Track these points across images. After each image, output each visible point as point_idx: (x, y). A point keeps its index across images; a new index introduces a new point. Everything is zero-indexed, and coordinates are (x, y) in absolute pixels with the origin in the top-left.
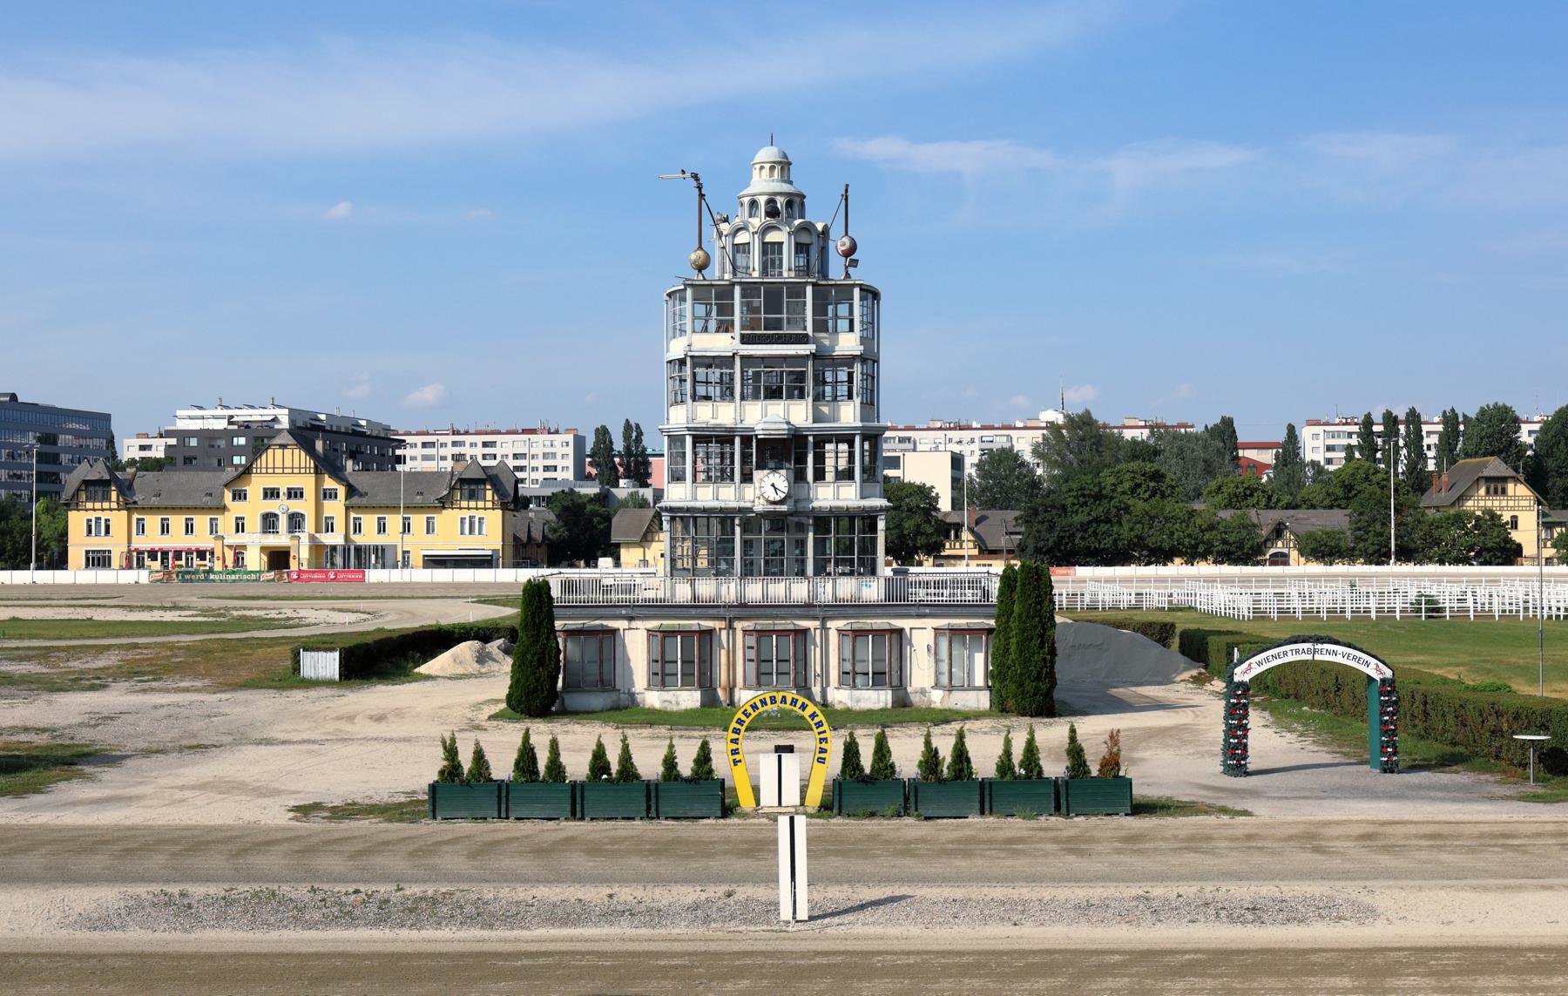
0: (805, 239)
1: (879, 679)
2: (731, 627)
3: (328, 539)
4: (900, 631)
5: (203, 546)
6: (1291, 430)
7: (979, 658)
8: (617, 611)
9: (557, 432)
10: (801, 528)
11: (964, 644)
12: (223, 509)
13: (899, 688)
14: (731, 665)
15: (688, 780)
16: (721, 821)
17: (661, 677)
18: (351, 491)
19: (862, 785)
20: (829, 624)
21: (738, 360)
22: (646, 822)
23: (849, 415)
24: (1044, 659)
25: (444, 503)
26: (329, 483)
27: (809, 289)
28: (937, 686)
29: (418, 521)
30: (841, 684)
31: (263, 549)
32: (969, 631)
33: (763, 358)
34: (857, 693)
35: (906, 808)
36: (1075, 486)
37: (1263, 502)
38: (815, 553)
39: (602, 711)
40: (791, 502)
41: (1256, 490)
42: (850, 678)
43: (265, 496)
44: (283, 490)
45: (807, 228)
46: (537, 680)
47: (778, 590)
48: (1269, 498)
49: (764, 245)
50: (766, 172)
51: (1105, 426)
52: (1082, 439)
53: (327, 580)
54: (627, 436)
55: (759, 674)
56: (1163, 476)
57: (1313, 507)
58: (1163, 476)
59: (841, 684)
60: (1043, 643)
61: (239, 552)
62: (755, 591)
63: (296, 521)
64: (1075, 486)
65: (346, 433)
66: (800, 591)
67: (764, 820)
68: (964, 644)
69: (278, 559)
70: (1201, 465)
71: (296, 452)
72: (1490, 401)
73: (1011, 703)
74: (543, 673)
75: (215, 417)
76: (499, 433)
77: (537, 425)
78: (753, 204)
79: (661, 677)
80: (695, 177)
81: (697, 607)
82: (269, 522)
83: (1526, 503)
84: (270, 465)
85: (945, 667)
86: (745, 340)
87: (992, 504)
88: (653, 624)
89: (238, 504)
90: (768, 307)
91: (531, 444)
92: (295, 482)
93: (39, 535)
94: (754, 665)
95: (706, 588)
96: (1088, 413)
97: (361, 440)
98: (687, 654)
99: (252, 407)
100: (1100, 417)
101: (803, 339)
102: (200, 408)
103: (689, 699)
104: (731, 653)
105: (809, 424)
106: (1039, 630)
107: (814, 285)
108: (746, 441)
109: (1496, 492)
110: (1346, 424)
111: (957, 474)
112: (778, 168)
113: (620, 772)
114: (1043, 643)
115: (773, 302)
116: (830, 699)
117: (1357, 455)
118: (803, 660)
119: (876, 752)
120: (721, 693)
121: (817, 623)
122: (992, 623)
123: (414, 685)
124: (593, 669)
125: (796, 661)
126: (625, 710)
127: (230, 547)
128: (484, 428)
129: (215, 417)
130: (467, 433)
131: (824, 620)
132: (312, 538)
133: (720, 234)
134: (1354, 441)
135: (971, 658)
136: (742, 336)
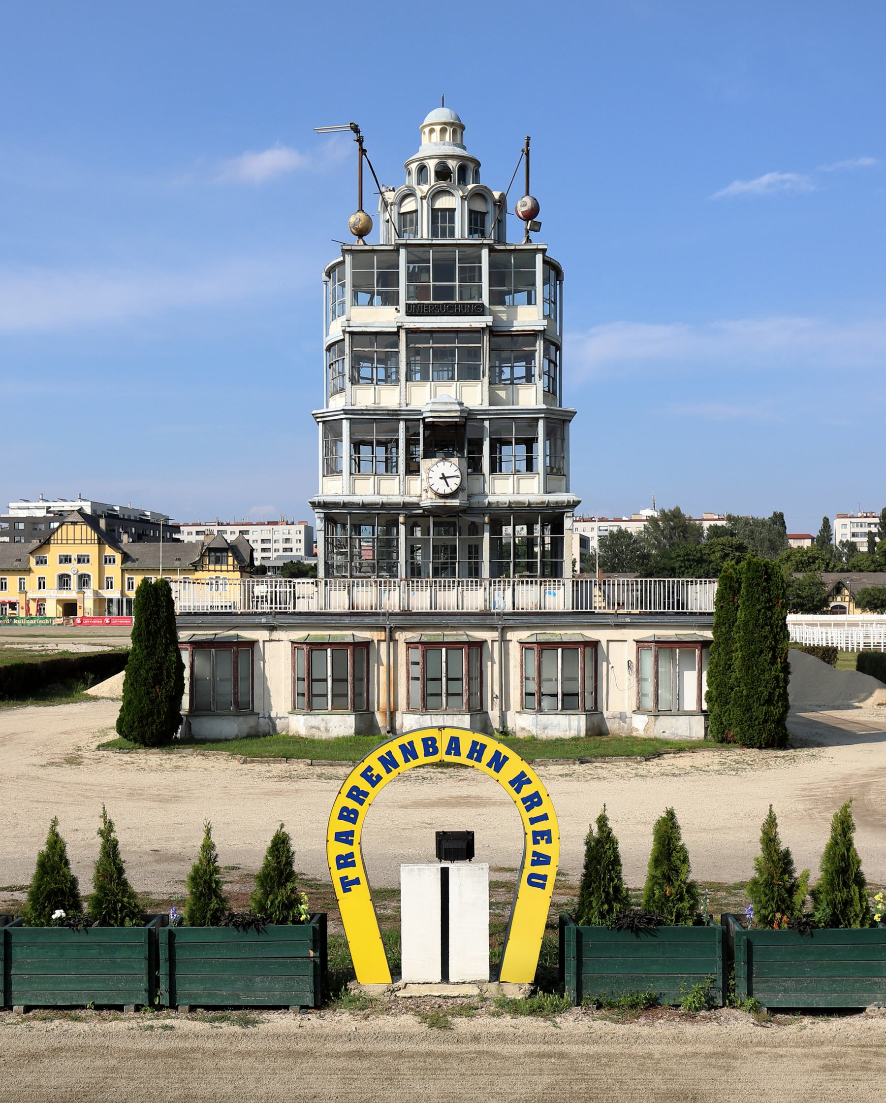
0: (479, 206)
1: (569, 701)
2: (391, 639)
3: (107, 594)
4: (594, 645)
5: (13, 600)
6: (826, 522)
7: (690, 678)
8: (257, 620)
9: (293, 524)
10: (475, 530)
11: (673, 658)
12: (29, 571)
13: (594, 712)
14: (392, 684)
15: (245, 924)
16: (314, 1021)
17: (308, 698)
18: (126, 557)
19: (627, 937)
20: (510, 635)
21: (403, 335)
22: (148, 1019)
23: (530, 397)
24: (777, 678)
25: (196, 566)
26: (109, 551)
27: (485, 253)
28: (639, 710)
30: (524, 707)
31: (59, 601)
32: (680, 643)
33: (431, 332)
34: (543, 719)
35: (727, 989)
36: (682, 553)
37: (823, 567)
38: (492, 556)
39: (236, 738)
40: (463, 496)
41: (817, 558)
42: (534, 700)
43: (61, 562)
44: (74, 557)
45: (481, 194)
46: (152, 701)
47: (449, 599)
48: (828, 565)
49: (434, 212)
50: (436, 136)
51: (690, 519)
52: (673, 528)
53: (104, 624)
55: (425, 696)
56: (746, 548)
57: (861, 571)
58: (746, 548)
59: (525, 707)
60: (774, 657)
61: (41, 604)
62: (420, 600)
63: (84, 580)
64: (682, 553)
65: (135, 521)
66: (474, 599)
67: (408, 1022)
68: (673, 658)
70: (767, 544)
71: (84, 527)
73: (734, 731)
74: (160, 692)
75: (37, 508)
76: (252, 524)
77: (279, 519)
78: (422, 169)
79: (308, 698)
80: (356, 129)
81: (355, 616)
82: (64, 581)
84: (64, 537)
85: (649, 688)
86: (412, 311)
87: (613, 569)
88: (299, 635)
89: (40, 567)
90: (440, 277)
91: (274, 533)
92: (83, 550)
94: (418, 684)
95: (366, 596)
96: (678, 510)
97: (146, 525)
98: (342, 670)
99: (65, 501)
100: (687, 512)
101: (478, 310)
102: (27, 501)
103: (342, 725)
104: (392, 671)
105: (486, 406)
106: (770, 642)
107: (492, 250)
110: (867, 517)
111: (584, 551)
112: (450, 130)
113: (97, 902)
114: (774, 657)
115: (444, 271)
116: (510, 725)
117: (877, 539)
118: (478, 678)
119: (657, 862)
120: (380, 720)
121: (495, 635)
122: (709, 634)
123: (84, 705)
124: (227, 688)
125: (470, 679)
126: (260, 740)
127: (34, 600)
128: (240, 521)
129: (37, 508)
130: (228, 524)
131: (504, 630)
132: (96, 593)
133: (386, 204)
134: (874, 530)
135: (680, 676)
136: (408, 306)
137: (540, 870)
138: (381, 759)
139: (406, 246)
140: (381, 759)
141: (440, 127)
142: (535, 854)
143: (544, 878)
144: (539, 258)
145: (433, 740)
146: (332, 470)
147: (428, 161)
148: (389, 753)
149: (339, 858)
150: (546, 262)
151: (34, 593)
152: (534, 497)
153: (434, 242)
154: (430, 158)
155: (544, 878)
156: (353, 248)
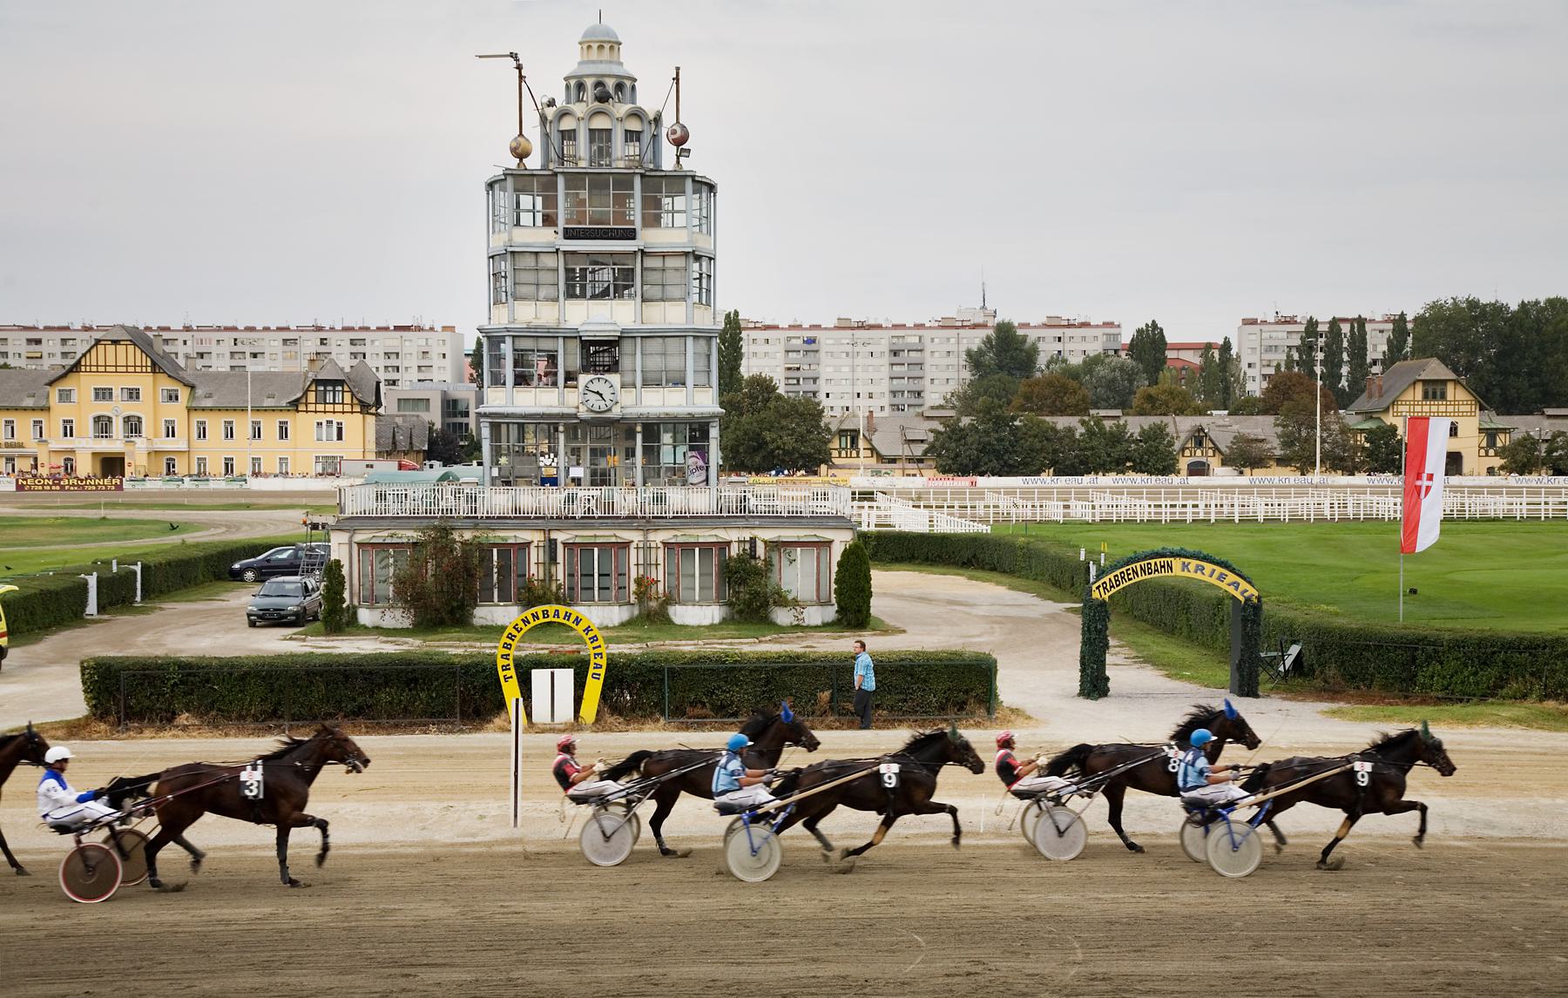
0: (634, 125)
29: (270, 425)
43: (97, 396)
45: (637, 114)
69: (112, 465)
72: (1430, 301)
80: (514, 56)
83: (1468, 408)
84: (101, 362)
86: (569, 234)
92: (132, 381)
93: (630, 453)
101: (630, 235)
107: (642, 176)
109: (1434, 397)
151: (58, 442)
154: (588, 76)
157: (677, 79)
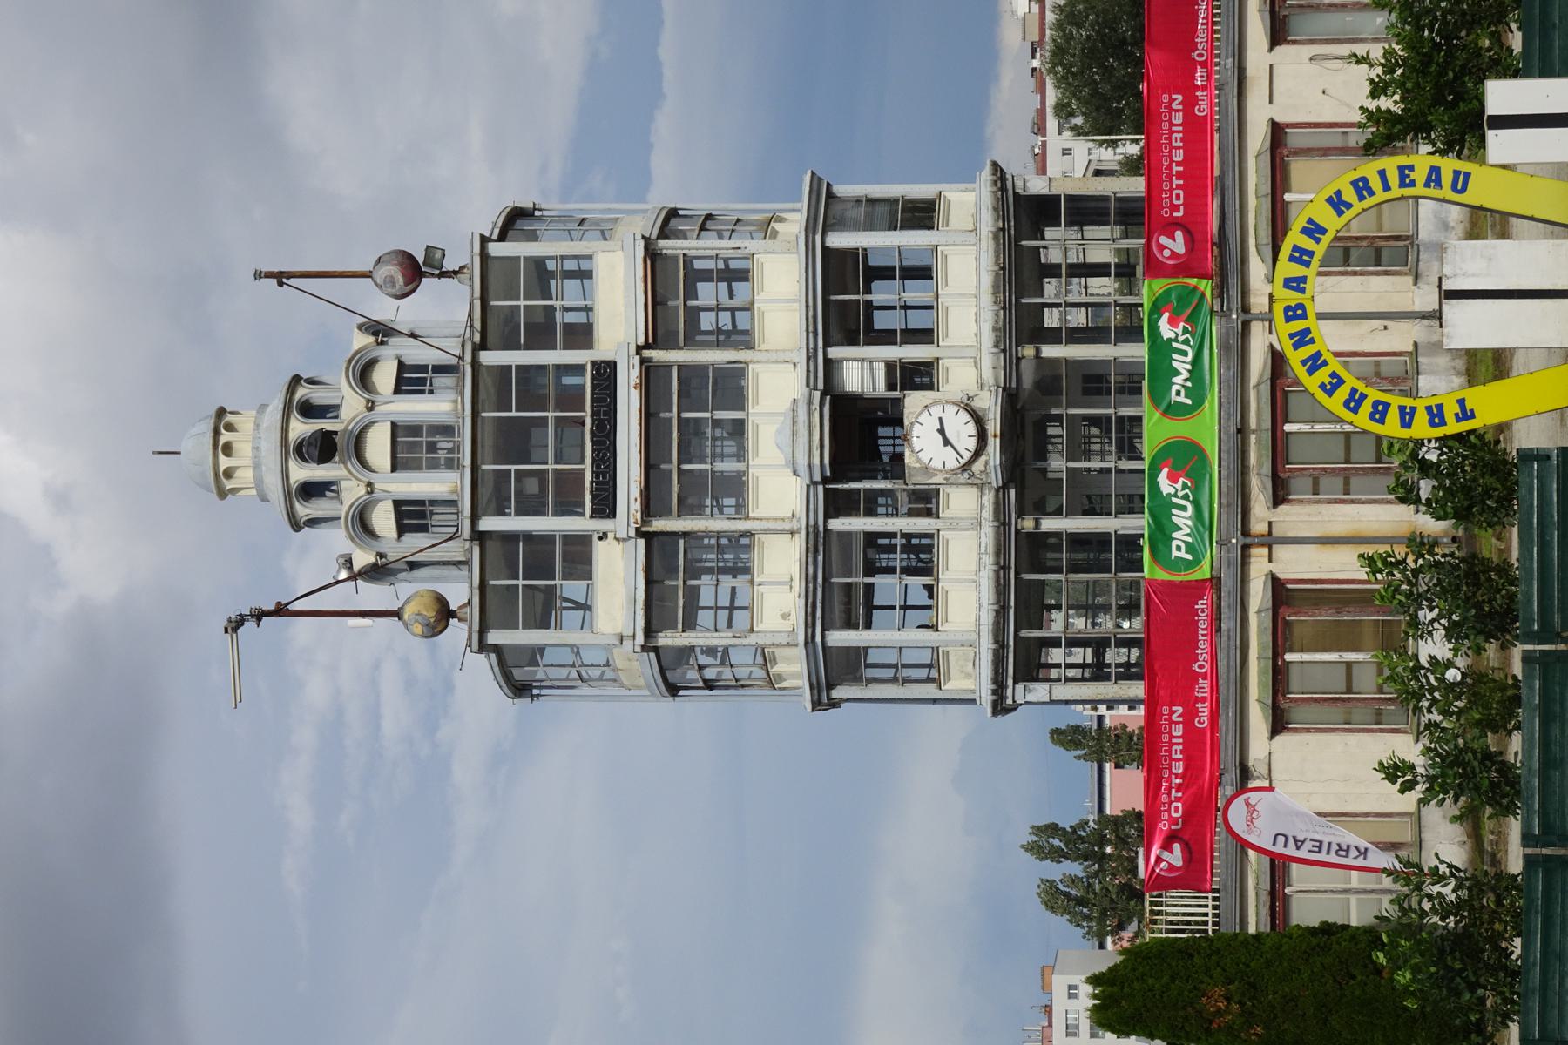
0: (385, 377)
33: (649, 467)
54: (1056, 855)
80: (235, 625)
86: (605, 506)
88: (1258, 721)
101: (605, 373)
108: (838, 504)
137: (1447, 178)
138: (1311, 372)
139: (474, 518)
140: (1311, 372)
141: (221, 457)
142: (1427, 185)
143: (1457, 173)
144: (496, 249)
145: (1287, 309)
146: (933, 669)
147: (292, 481)
148: (1304, 362)
149: (1432, 424)
150: (502, 237)
152: (984, 256)
153: (468, 461)
154: (286, 476)
155: (1457, 173)
156: (476, 627)
157: (281, 277)
